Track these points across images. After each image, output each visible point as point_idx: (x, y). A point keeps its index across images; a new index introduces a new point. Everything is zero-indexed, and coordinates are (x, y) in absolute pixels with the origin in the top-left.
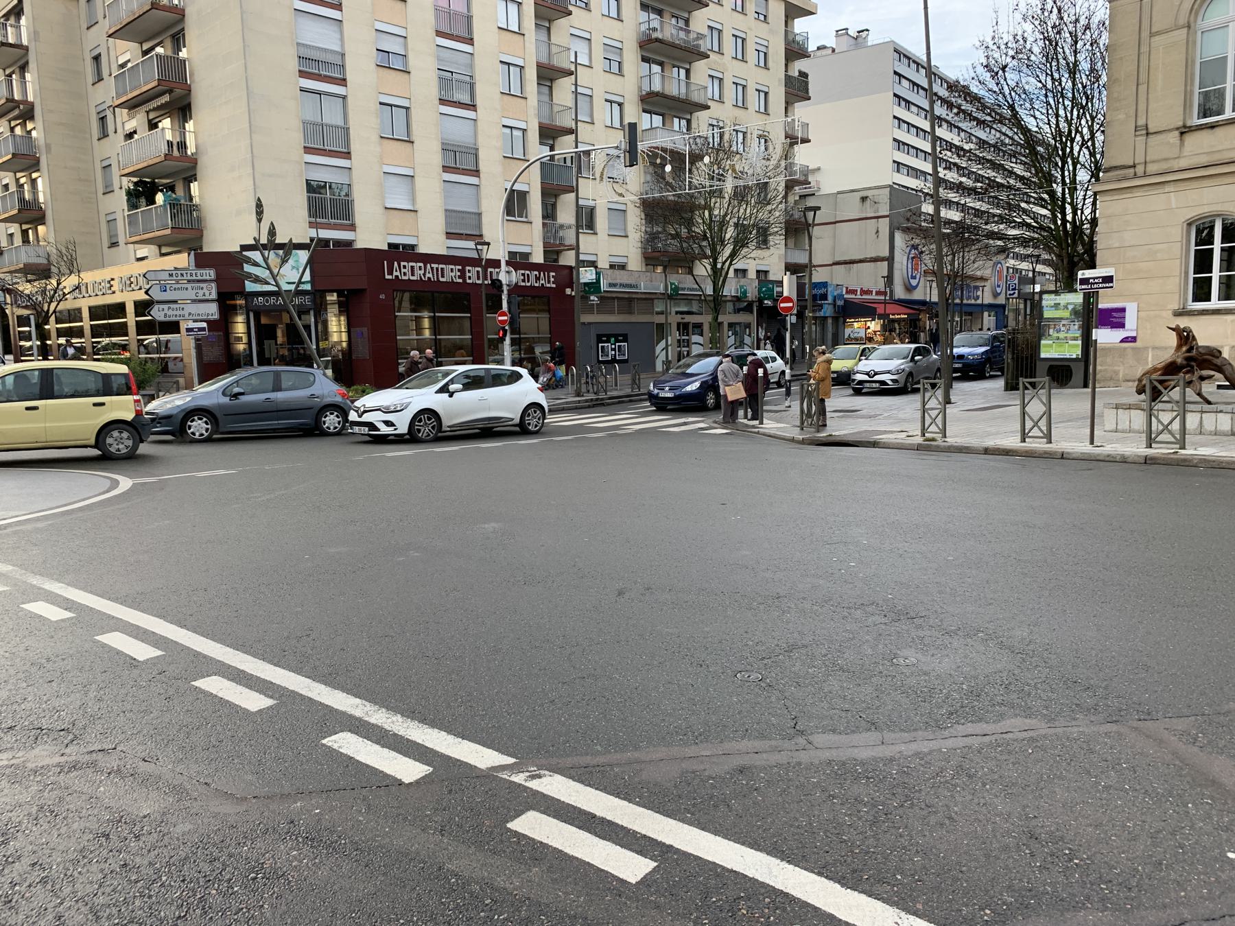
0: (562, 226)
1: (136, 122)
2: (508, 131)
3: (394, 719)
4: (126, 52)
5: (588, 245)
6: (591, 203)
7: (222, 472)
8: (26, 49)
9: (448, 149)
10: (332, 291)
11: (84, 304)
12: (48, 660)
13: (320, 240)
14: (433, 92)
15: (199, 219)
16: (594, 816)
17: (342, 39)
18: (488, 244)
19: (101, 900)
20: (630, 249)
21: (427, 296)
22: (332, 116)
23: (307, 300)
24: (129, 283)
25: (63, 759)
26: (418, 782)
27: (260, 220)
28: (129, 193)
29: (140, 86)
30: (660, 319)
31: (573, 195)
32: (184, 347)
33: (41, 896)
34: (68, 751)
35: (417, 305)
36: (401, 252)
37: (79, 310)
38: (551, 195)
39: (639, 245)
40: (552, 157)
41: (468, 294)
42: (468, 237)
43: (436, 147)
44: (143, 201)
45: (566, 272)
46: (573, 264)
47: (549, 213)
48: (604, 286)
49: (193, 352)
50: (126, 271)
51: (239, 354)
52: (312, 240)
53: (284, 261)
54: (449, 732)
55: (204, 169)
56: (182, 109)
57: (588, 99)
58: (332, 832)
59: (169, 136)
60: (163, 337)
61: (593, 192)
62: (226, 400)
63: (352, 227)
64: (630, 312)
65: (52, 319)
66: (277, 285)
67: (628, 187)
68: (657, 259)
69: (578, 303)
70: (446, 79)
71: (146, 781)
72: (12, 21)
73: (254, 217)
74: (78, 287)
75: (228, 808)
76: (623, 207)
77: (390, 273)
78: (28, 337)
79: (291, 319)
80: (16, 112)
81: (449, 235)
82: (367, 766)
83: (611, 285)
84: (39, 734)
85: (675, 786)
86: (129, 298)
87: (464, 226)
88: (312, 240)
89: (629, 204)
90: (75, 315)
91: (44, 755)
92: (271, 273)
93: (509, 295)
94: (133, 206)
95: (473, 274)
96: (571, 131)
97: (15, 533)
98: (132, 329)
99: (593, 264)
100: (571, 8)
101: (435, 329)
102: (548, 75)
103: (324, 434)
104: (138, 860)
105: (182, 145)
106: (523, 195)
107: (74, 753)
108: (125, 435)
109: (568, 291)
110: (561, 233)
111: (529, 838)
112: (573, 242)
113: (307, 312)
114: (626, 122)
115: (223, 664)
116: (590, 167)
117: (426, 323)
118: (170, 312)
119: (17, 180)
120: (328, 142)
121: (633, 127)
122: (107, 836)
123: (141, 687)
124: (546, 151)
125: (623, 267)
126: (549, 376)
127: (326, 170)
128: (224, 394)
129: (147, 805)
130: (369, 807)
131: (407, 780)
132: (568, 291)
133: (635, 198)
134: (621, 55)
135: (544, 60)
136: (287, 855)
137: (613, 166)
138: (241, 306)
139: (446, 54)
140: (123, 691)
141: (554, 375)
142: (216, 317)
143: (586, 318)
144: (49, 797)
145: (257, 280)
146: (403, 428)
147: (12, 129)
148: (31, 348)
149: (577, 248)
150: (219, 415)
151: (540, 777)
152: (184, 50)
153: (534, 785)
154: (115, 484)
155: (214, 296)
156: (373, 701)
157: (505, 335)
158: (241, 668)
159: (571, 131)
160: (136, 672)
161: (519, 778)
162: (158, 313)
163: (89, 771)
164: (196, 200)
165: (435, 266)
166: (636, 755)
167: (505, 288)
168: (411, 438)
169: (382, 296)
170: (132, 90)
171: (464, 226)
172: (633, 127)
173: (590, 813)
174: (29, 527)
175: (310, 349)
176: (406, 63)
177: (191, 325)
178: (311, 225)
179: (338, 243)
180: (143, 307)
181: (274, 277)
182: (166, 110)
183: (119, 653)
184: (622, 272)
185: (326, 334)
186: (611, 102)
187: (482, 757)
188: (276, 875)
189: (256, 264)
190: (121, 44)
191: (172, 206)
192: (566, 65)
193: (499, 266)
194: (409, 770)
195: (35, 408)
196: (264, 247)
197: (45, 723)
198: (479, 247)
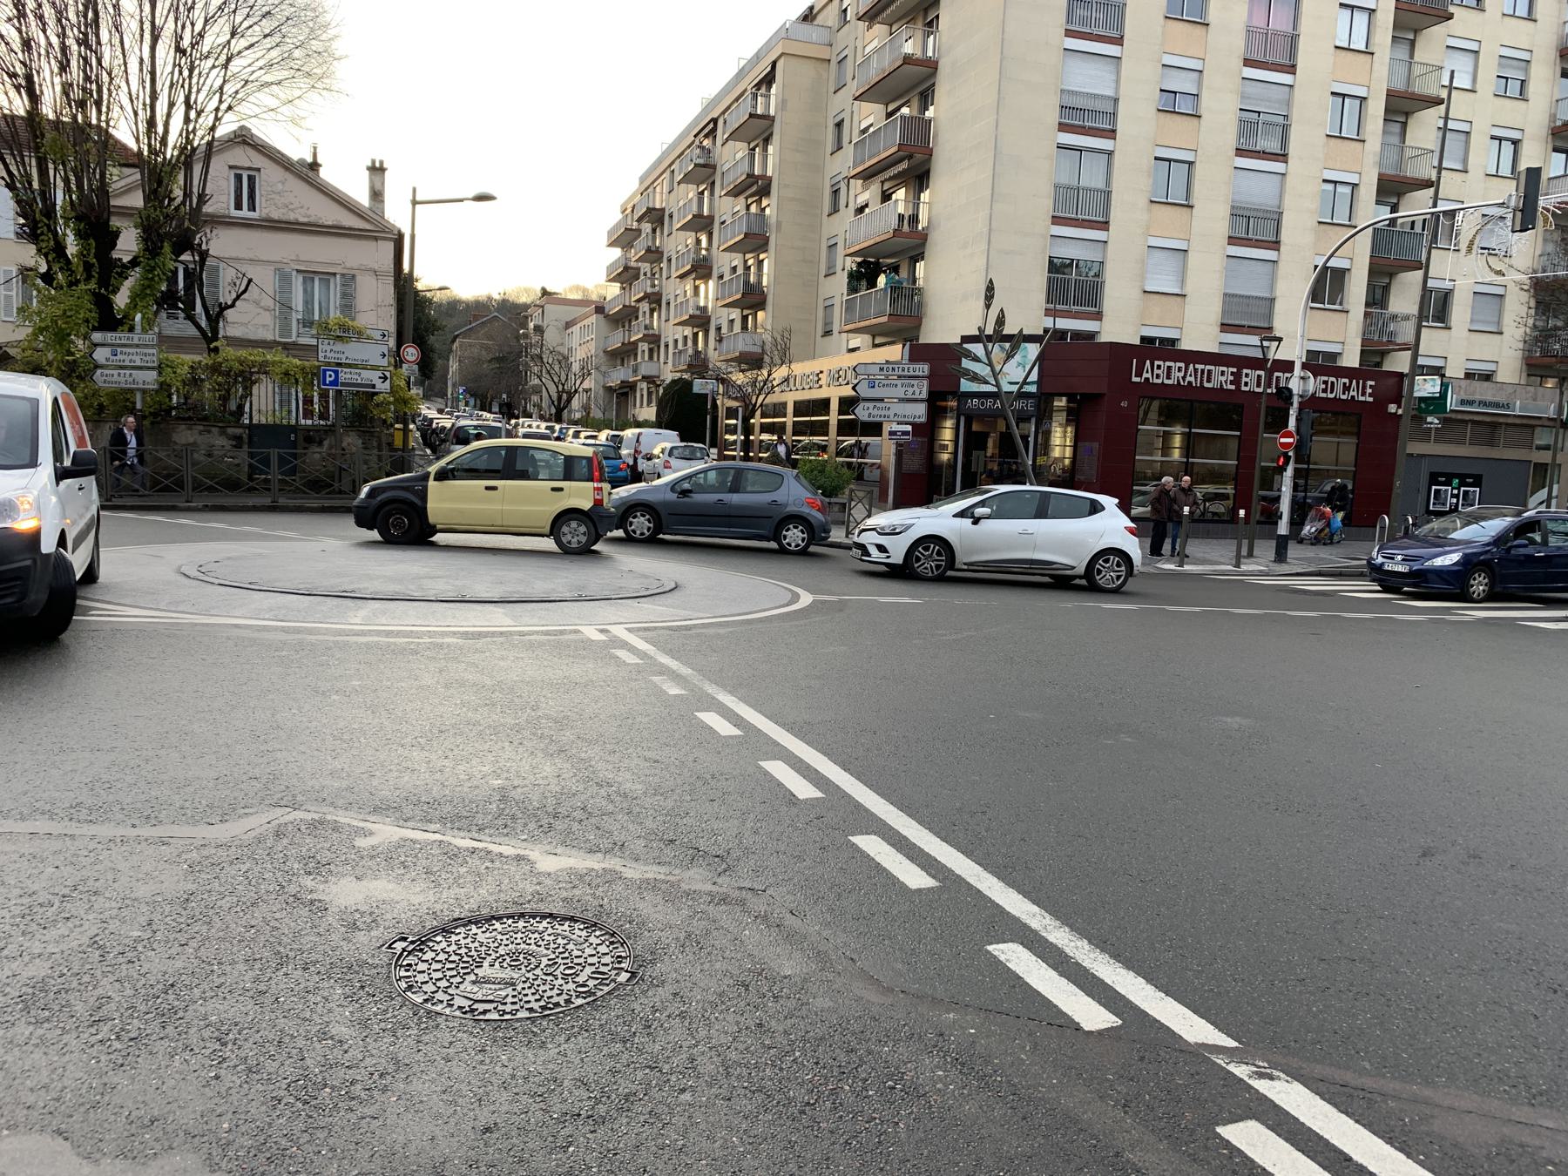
0: (1394, 317)
1: (867, 194)
2: (1330, 187)
3: (1079, 944)
4: (871, 115)
5: (1433, 343)
6: (1447, 285)
7: (907, 600)
8: (772, 119)
9: (1238, 214)
10: (1062, 395)
11: (790, 398)
12: (713, 777)
13: (1056, 331)
14: (1230, 139)
15: (920, 305)
16: (1349, 1159)
17: (1118, 81)
18: (1280, 340)
19: (734, 1055)
20: (1504, 353)
21: (1181, 406)
22: (1092, 177)
23: (1029, 405)
24: (836, 377)
25: (715, 889)
26: (1100, 1033)
27: (988, 307)
28: (851, 275)
29: (879, 153)
30: (1545, 457)
31: (1420, 273)
32: (884, 451)
33: (678, 1031)
34: (720, 881)
35: (1169, 416)
36: (1158, 348)
37: (784, 405)
38: (1382, 274)
39: (1521, 345)
40: (1393, 222)
41: (1242, 406)
42: (1251, 330)
43: (1223, 212)
44: (864, 283)
45: (1392, 381)
46: (1406, 371)
47: (1377, 297)
48: (1451, 402)
49: (893, 459)
50: (835, 363)
51: (941, 466)
52: (1046, 331)
53: (1009, 356)
54: (1149, 980)
55: (934, 248)
56: (919, 178)
57: (1462, 137)
58: (987, 1063)
59: (901, 209)
60: (865, 440)
61: (1452, 268)
62: (673, 497)
63: (1098, 316)
64: (1491, 443)
65: (758, 413)
66: (998, 385)
67: (1513, 261)
68: (1548, 367)
69: (1405, 427)
70: (1249, 122)
71: (792, 938)
72: (763, 91)
73: (981, 302)
74: (787, 380)
75: (873, 996)
76: (1500, 291)
77: (1139, 374)
78: (734, 432)
79: (1008, 426)
80: (754, 188)
81: (1226, 327)
82: (1039, 993)
83: (1463, 402)
84: (696, 855)
85: (1488, 1157)
86: (835, 393)
87: (1249, 315)
88: (1046, 331)
89: (1511, 286)
90: (779, 409)
91: (697, 879)
92: (993, 370)
93: (1300, 409)
94: (853, 289)
95: (1251, 380)
96: (1427, 184)
97: (698, 635)
98: (789, 429)
99: (1438, 371)
100: (1452, 9)
101: (1188, 450)
102: (1402, 106)
103: (783, 551)
104: (773, 1023)
105: (914, 219)
106: (1340, 275)
107: (726, 884)
108: (583, 529)
109: (1392, 408)
110: (1392, 327)
111: (1246, 1156)
112: (1410, 338)
113: (1028, 420)
114: (1523, 166)
115: (885, 824)
116: (1452, 233)
117: (1177, 441)
118: (876, 412)
119: (746, 261)
120: (1084, 209)
121: (1534, 174)
122: (747, 987)
123: (797, 828)
124: (1385, 213)
125: (1487, 377)
126: (1320, 525)
127: (1075, 245)
128: (673, 489)
129: (790, 965)
130: (1035, 1046)
131: (1087, 1026)
132: (1392, 408)
133: (1524, 278)
134: (1527, 71)
135: (1399, 86)
136: (930, 1071)
137: (1492, 231)
138: (952, 410)
139: (1252, 88)
140: (779, 829)
141: (1328, 525)
142: (923, 419)
143: (1415, 448)
144: (698, 926)
145: (975, 378)
146: (897, 557)
147: (748, 207)
148: (735, 442)
149: (1415, 348)
150: (663, 514)
151: (1271, 1078)
152: (931, 108)
153: (1262, 1086)
154: (795, 598)
155: (924, 395)
156: (1055, 914)
157: (1287, 463)
158: (905, 833)
159: (1427, 184)
160: (794, 811)
161: (1241, 1071)
162: (863, 413)
163: (738, 909)
164: (920, 283)
166: (1427, 1092)
167: (1296, 400)
168: (902, 572)
169: (1124, 404)
170: (870, 158)
171: (1249, 315)
172: (1534, 174)
173: (1341, 1153)
174: (712, 631)
175: (1025, 465)
176: (1197, 106)
177: (895, 427)
178: (1048, 313)
179: (1077, 335)
180: (847, 404)
181: (995, 375)
182: (902, 179)
183: (780, 784)
184: (1486, 384)
185: (1046, 447)
186: (1500, 139)
187: (1193, 1028)
188: (914, 1092)
189: (976, 359)
190: (867, 107)
191: (894, 289)
192: (1433, 91)
193: (1292, 371)
194: (1092, 1016)
195: (494, 488)
196: (989, 338)
197: (702, 844)
198: (1265, 343)
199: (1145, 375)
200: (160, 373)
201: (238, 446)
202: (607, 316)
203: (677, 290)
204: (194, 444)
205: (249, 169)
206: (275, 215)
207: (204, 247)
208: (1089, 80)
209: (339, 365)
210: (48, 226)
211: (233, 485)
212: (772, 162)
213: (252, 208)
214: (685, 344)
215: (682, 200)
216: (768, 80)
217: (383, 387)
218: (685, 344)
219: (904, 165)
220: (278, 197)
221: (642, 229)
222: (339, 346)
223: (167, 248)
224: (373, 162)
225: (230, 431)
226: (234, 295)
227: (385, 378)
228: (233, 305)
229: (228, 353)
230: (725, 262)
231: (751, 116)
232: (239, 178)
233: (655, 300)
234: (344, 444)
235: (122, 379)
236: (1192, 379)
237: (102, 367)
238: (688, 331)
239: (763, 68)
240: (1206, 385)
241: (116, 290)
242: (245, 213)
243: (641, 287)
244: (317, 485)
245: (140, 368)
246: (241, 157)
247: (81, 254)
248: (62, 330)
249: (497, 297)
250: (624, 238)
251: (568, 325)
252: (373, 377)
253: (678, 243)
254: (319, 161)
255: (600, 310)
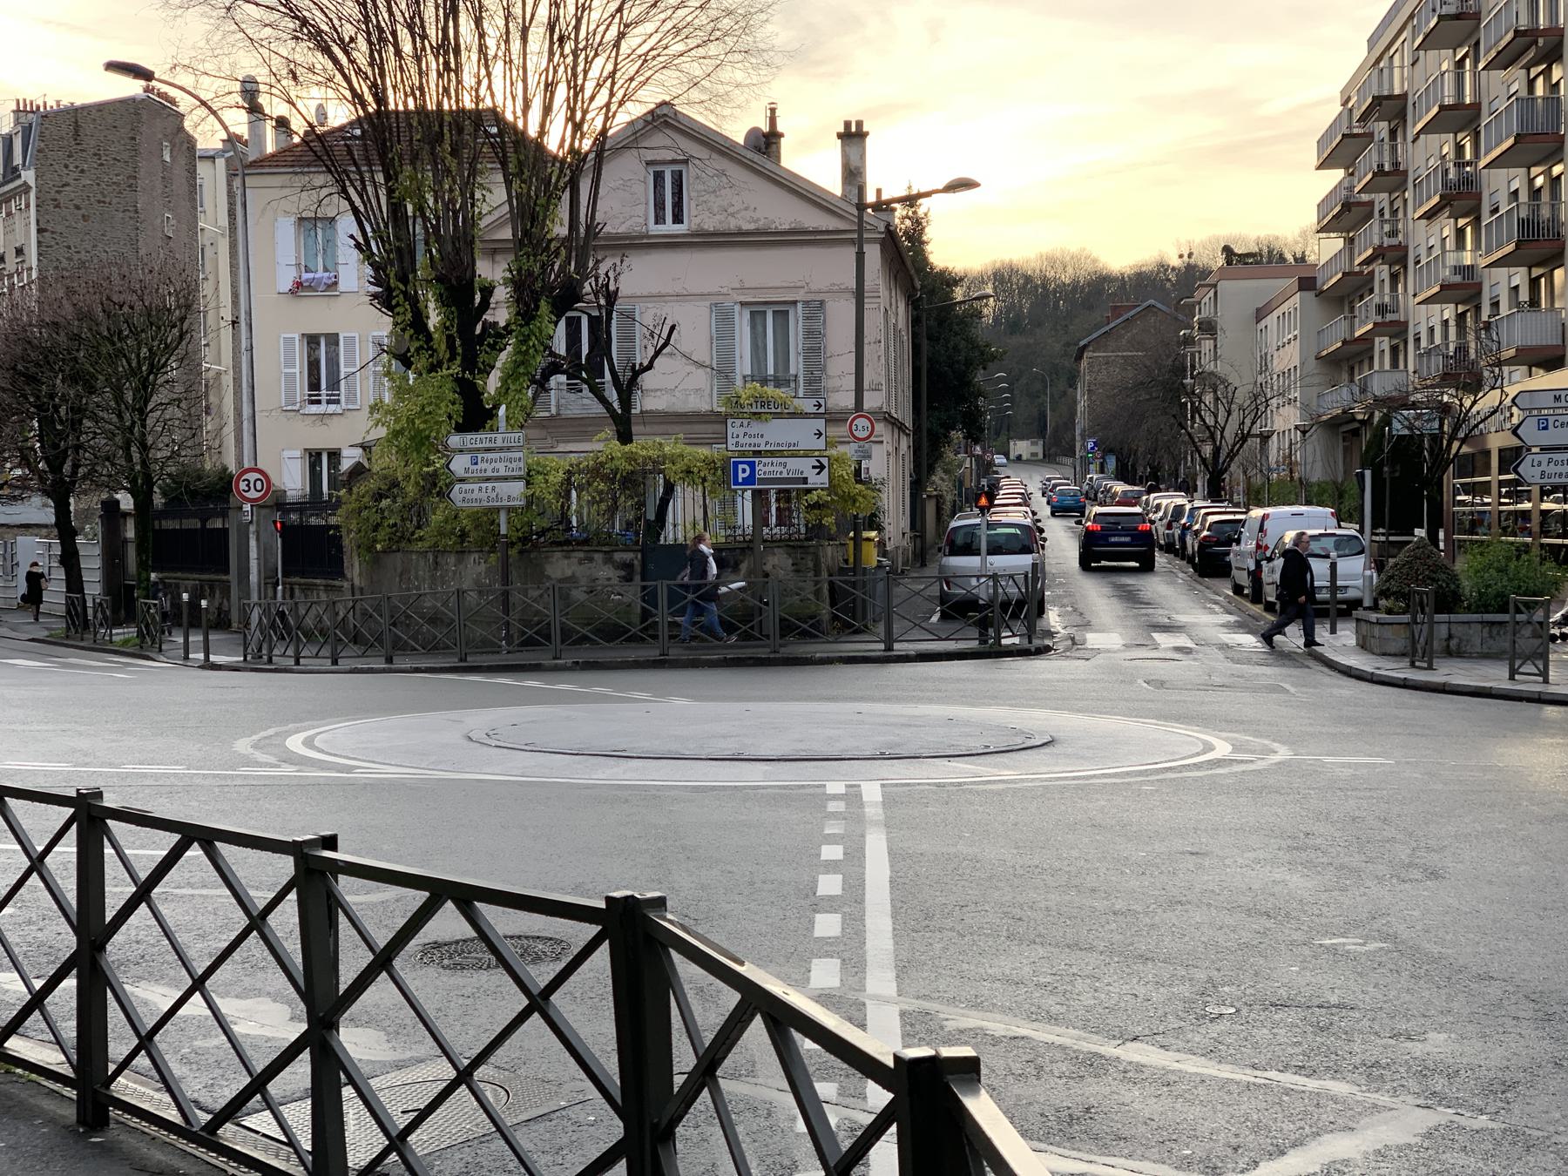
80: (1531, 54)
118: (1552, 469)
119: (1531, 181)
200: (528, 483)
201: (628, 579)
202: (1320, 294)
205: (674, 162)
207: (612, 288)
209: (758, 453)
210: (405, 293)
211: (612, 633)
213: (678, 219)
214: (1446, 336)
215: (1431, 77)
217: (818, 480)
218: (1446, 336)
220: (714, 201)
222: (756, 428)
223: (544, 307)
224: (847, 124)
225: (618, 556)
226: (651, 352)
227: (822, 467)
228: (650, 366)
230: (1503, 186)
232: (659, 177)
233: (1396, 256)
234: (768, 568)
235: (483, 495)
237: (462, 480)
238: (1449, 312)
242: (669, 227)
243: (1373, 234)
245: (505, 479)
246: (663, 146)
248: (419, 431)
249: (1175, 262)
250: (1341, 149)
251: (1260, 314)
252: (805, 466)
253: (1429, 154)
254: (780, 128)
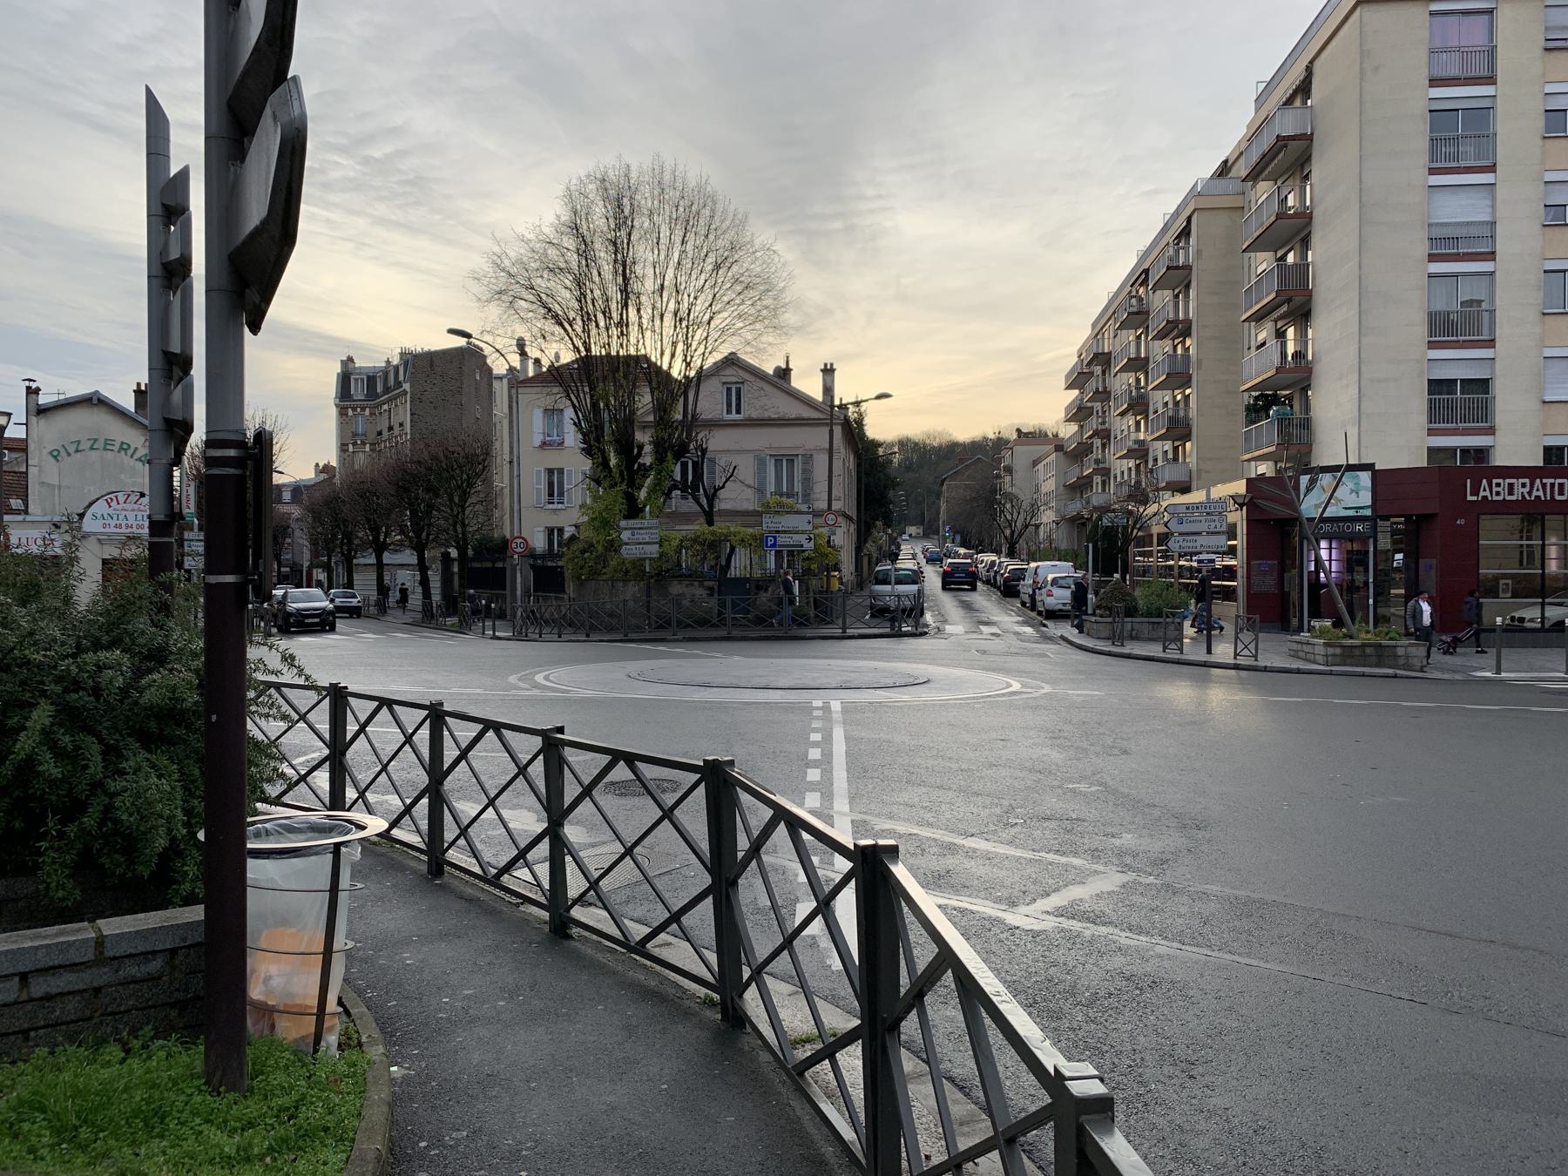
17: (1493, 207)
63: (1491, 431)
77: (1475, 492)
127: (1458, 363)
165: (1548, 481)
199: (1482, 493)
201: (711, 595)
203: (1124, 426)
204: (683, 595)
206: (755, 415)
208: (1460, 209)
211: (703, 622)
212: (1192, 308)
213: (738, 412)
216: (1185, 233)
219: (1284, 308)
221: (1091, 372)
222: (777, 518)
229: (720, 526)
230: (1160, 399)
231: (1168, 268)
232: (729, 390)
233: (1105, 435)
236: (1541, 493)
238: (1132, 463)
239: (1180, 223)
240: (1558, 498)
241: (640, 487)
242: (734, 416)
243: (1093, 423)
244: (760, 621)
246: (731, 375)
247: (618, 465)
249: (992, 436)
250: (1077, 380)
251: (1035, 463)
252: (802, 539)
253: (1122, 383)
255: (1059, 448)
